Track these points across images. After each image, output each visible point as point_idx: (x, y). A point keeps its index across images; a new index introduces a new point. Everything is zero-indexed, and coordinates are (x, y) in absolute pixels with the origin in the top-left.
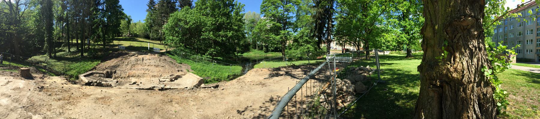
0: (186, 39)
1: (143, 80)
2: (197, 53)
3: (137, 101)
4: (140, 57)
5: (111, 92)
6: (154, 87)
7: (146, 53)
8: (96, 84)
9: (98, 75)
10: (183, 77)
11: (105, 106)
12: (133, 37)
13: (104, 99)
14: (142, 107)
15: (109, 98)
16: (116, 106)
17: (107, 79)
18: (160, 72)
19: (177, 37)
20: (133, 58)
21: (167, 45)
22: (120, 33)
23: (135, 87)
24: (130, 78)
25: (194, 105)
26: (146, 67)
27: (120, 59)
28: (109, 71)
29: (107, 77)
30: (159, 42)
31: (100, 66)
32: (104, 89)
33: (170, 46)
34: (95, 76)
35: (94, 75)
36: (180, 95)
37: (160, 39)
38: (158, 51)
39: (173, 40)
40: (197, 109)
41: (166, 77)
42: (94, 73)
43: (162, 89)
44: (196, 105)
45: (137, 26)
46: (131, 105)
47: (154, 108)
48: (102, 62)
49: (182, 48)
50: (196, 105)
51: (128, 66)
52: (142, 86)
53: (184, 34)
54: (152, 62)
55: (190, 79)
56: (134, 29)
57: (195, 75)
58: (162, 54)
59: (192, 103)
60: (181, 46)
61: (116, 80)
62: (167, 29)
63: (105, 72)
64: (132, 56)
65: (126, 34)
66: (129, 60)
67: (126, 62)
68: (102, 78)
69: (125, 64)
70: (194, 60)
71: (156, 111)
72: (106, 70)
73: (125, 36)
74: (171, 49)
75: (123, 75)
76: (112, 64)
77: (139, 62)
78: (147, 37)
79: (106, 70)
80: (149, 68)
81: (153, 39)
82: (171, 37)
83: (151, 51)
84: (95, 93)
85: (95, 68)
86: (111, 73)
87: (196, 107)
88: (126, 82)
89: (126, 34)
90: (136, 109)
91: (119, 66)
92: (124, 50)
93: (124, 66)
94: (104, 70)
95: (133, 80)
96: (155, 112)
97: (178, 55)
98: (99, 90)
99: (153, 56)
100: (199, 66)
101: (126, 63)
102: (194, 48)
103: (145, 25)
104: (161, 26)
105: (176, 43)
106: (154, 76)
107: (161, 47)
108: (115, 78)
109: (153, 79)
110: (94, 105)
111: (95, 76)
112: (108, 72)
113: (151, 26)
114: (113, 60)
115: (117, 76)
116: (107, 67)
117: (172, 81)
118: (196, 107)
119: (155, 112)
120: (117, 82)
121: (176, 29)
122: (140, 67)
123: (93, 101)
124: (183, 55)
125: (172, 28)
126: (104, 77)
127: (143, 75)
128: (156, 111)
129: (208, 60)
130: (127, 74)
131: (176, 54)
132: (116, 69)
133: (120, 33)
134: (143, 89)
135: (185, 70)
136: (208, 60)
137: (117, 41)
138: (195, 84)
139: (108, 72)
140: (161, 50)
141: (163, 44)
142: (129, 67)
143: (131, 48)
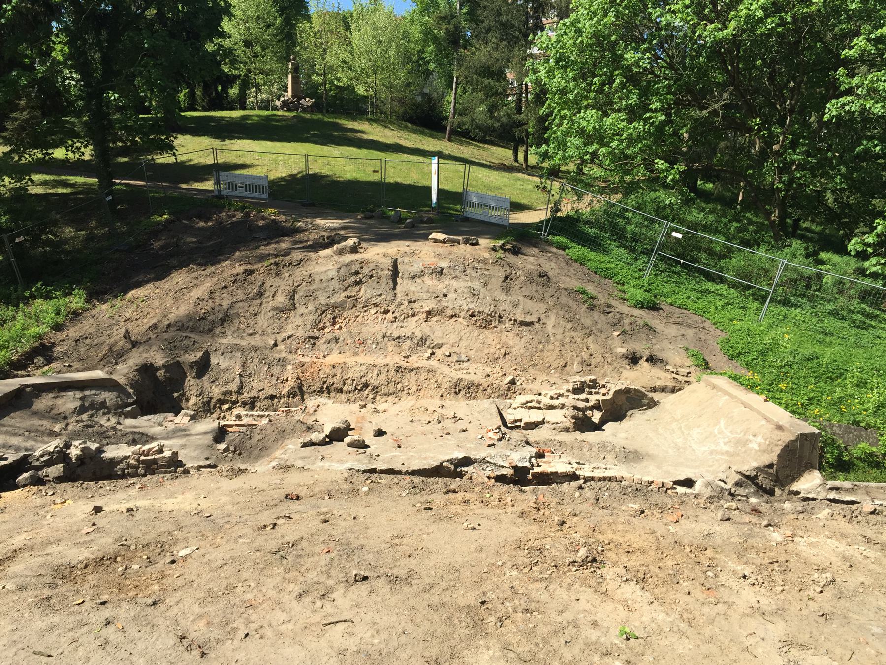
0: (701, 129)
1: (392, 413)
2: (784, 232)
3: (349, 551)
4: (378, 253)
5: (170, 504)
6: (467, 461)
7: (414, 232)
8: (57, 470)
9: (69, 402)
10: (667, 401)
11: (124, 612)
12: (326, 113)
13: (113, 569)
14: (382, 585)
15: (160, 548)
16: (212, 596)
17: (146, 423)
18: (507, 364)
19: (633, 114)
20: (325, 264)
21: (554, 173)
22: (229, 81)
23: (340, 461)
24: (311, 402)
25: (757, 611)
26: (414, 327)
27: (231, 268)
28: (159, 359)
29: (146, 408)
30: (504, 154)
31: (86, 326)
32: (116, 498)
33: (580, 182)
34: (50, 414)
35: (43, 403)
36: (654, 522)
37: (508, 134)
38: (493, 215)
39: (599, 137)
40: (788, 644)
41: (548, 397)
42: (40, 389)
43: (520, 477)
44: (780, 612)
45: (355, 37)
46: (312, 576)
47: (471, 598)
48: (96, 295)
49: (669, 199)
50: (780, 612)
51: (296, 319)
52: (384, 454)
53: (691, 93)
54: (458, 292)
55: (713, 424)
56: (336, 54)
57: (756, 400)
58: (522, 238)
59: (748, 596)
60: (656, 181)
61: (209, 424)
62: (562, 62)
63: (123, 372)
64: (317, 246)
65: (273, 92)
66: (300, 273)
67: (278, 290)
68: (107, 421)
69: (269, 304)
70: (749, 286)
71: (478, 615)
72: (135, 359)
73: (266, 105)
74: (586, 205)
75: (260, 384)
76: (180, 310)
77: (365, 292)
78: (426, 118)
79: (135, 359)
80: (437, 330)
81: (462, 135)
82: (589, 118)
83: (450, 216)
84: (45, 533)
85: (43, 352)
86: (176, 373)
87: (778, 630)
88: (283, 434)
89: (273, 92)
90: (344, 601)
91: (226, 319)
92: (260, 206)
93: (262, 321)
94: (116, 356)
95: (330, 413)
96: (478, 624)
97: (635, 245)
98: (74, 505)
99: (463, 250)
100: (785, 332)
101: (281, 299)
102: (760, 198)
103: (416, 32)
104: (518, 33)
105: (622, 161)
106: (465, 389)
107: (521, 187)
108: (207, 408)
109: (460, 406)
110: (40, 623)
111: (50, 414)
112: (147, 369)
113: (455, 40)
114: (179, 278)
115: (216, 392)
116: (137, 330)
117: (583, 424)
118: (778, 630)
119: (478, 624)
120: (221, 434)
121: (630, 56)
122: (373, 325)
123: (30, 596)
124: (669, 244)
125: (599, 58)
126: (119, 410)
127: (395, 383)
128: (478, 615)
129: (865, 296)
130: (290, 372)
131: (619, 235)
132: (207, 343)
133: (229, 81)
134: (391, 472)
135: (676, 357)
136: (865, 296)
137: (205, 142)
138: (749, 465)
139: (147, 369)
140: (517, 207)
141: (529, 170)
142: (298, 325)
143: (312, 194)
